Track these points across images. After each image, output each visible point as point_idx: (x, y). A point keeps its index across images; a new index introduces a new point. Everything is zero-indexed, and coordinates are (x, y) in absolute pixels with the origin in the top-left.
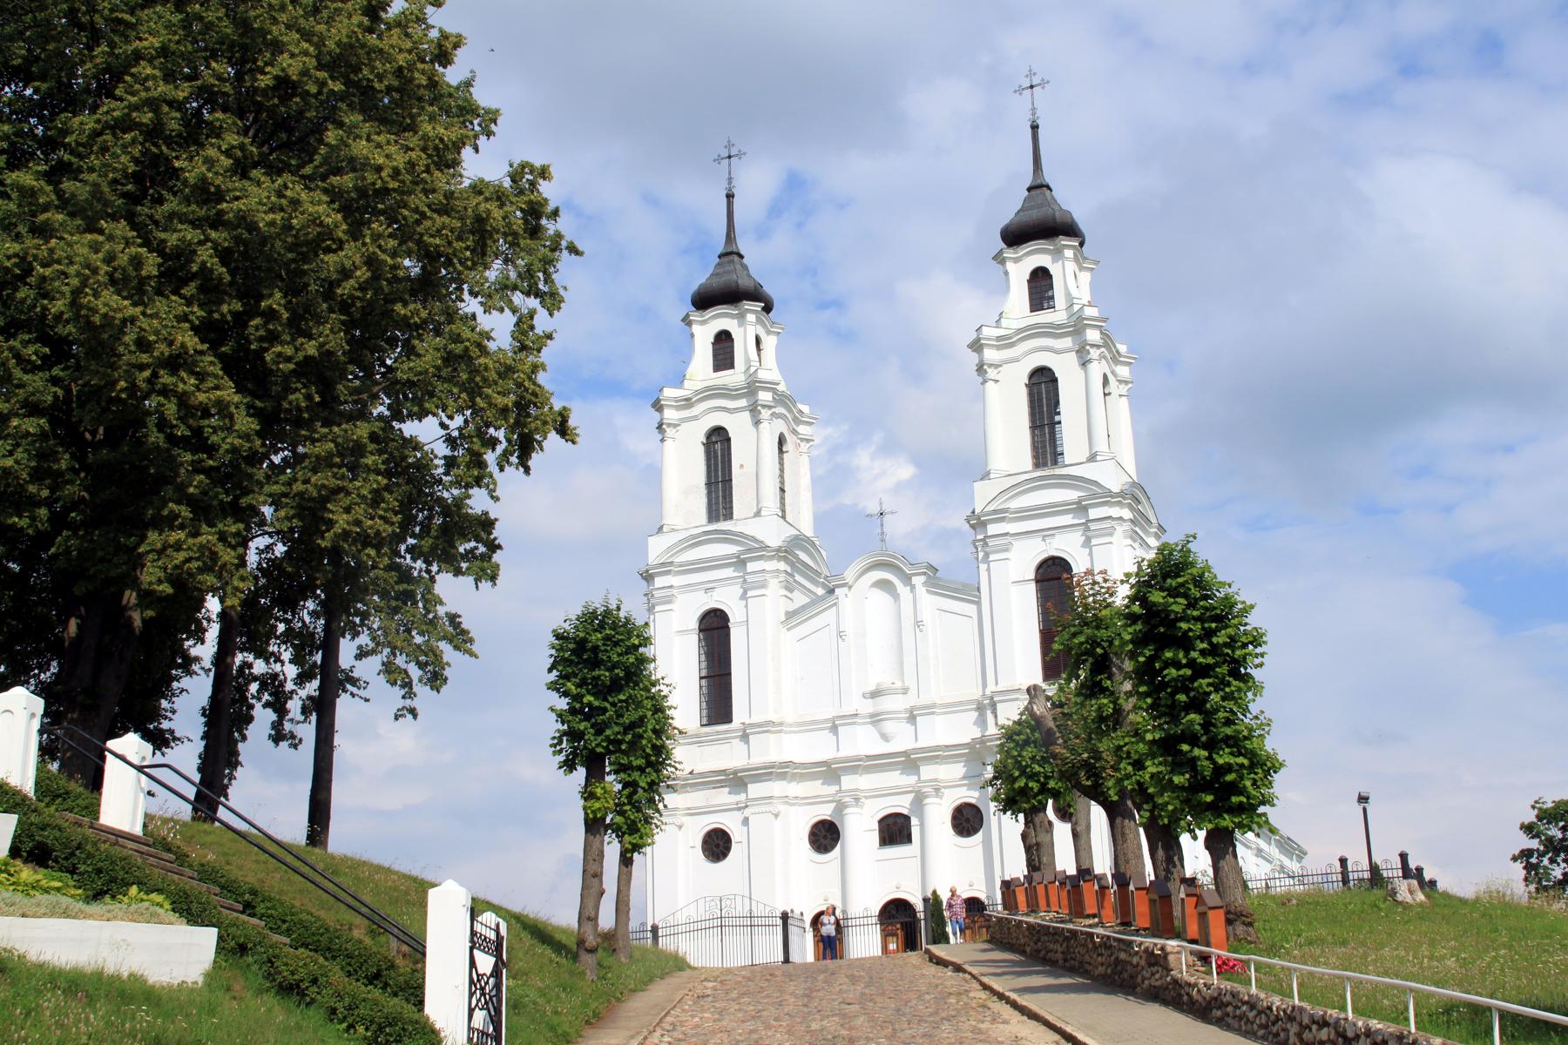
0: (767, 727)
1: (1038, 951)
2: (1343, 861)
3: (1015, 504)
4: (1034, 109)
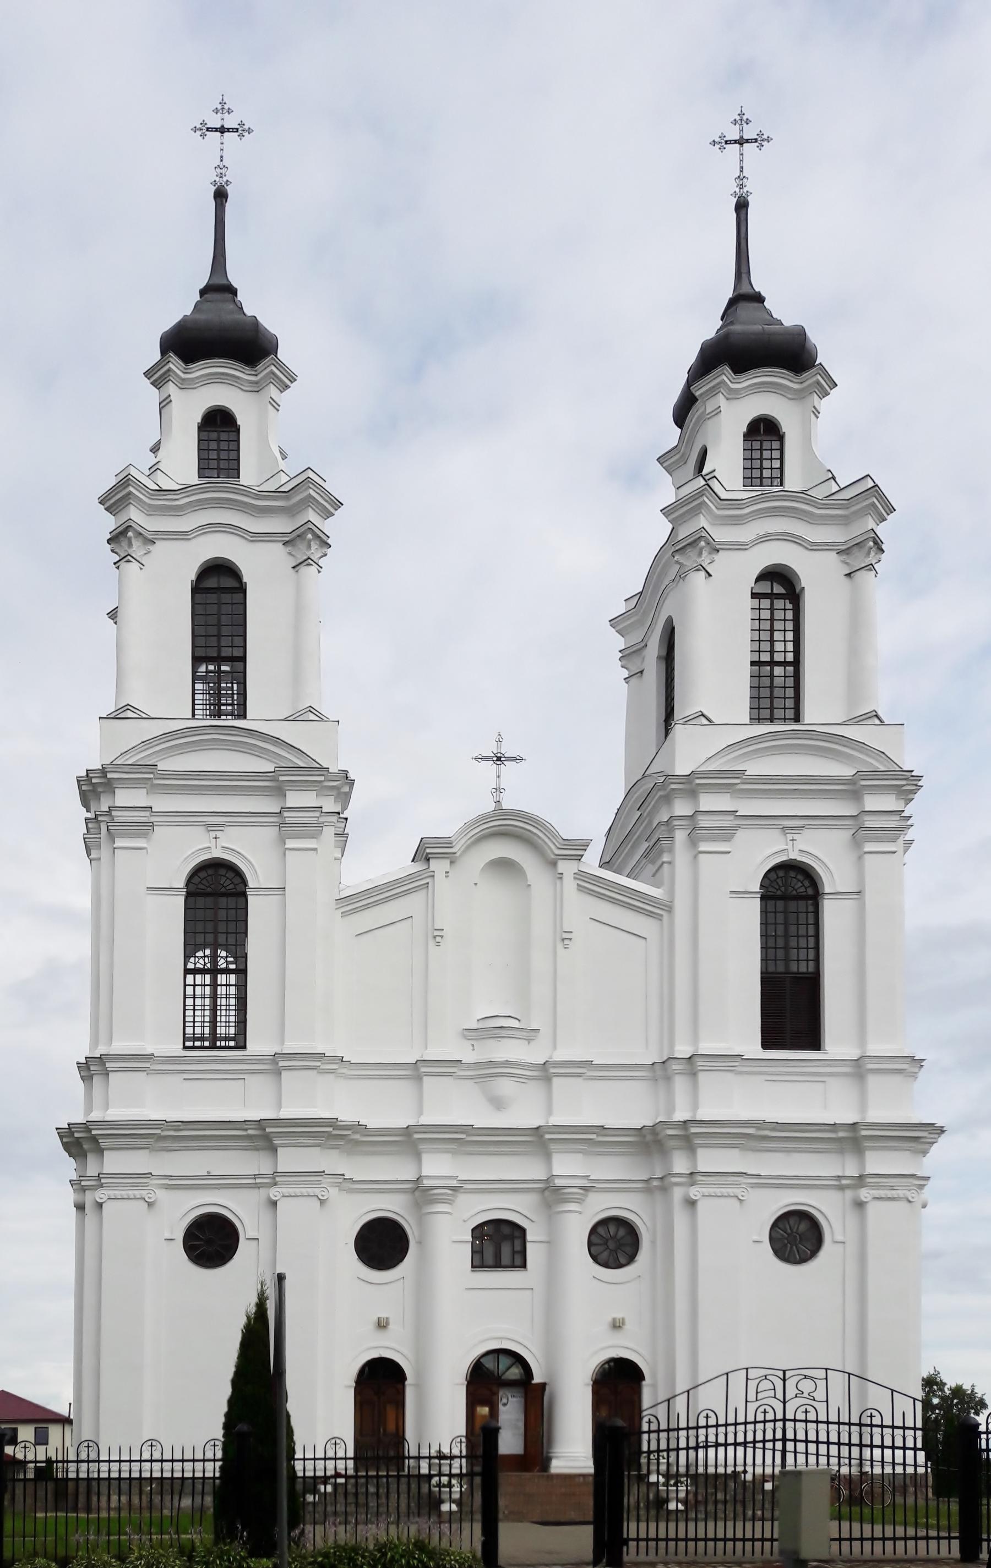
3: (756, 768)
4: (741, 178)
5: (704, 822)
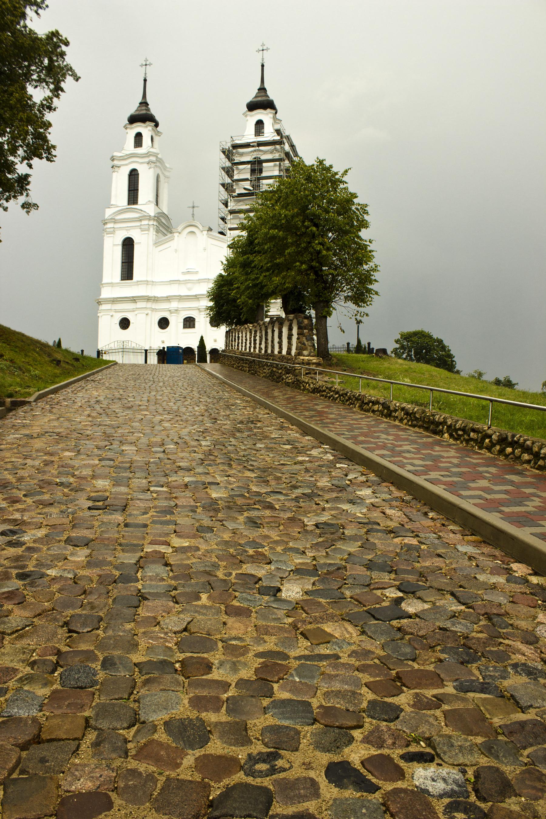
0: (147, 282)
1: (239, 367)
2: (348, 344)
4: (146, 74)
5: (142, 227)
